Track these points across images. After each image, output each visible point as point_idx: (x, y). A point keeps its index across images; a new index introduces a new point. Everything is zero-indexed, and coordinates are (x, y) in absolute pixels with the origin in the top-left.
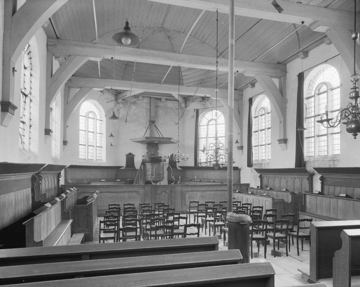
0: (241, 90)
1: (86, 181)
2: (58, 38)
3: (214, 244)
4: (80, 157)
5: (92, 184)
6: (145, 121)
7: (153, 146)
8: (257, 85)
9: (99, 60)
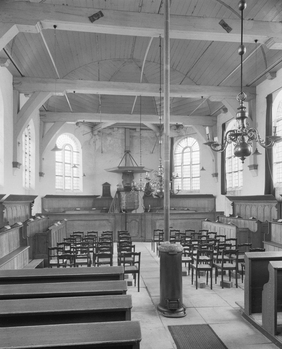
1: (62, 210)
2: (22, 76)
3: (118, 274)
4: (57, 187)
5: (67, 213)
6: (120, 151)
7: (128, 175)
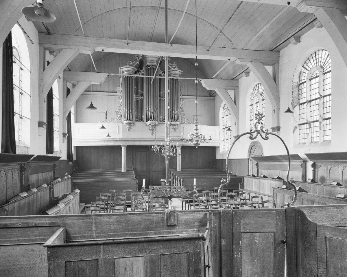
0: (237, 80)
8: (251, 73)
9: (90, 53)
